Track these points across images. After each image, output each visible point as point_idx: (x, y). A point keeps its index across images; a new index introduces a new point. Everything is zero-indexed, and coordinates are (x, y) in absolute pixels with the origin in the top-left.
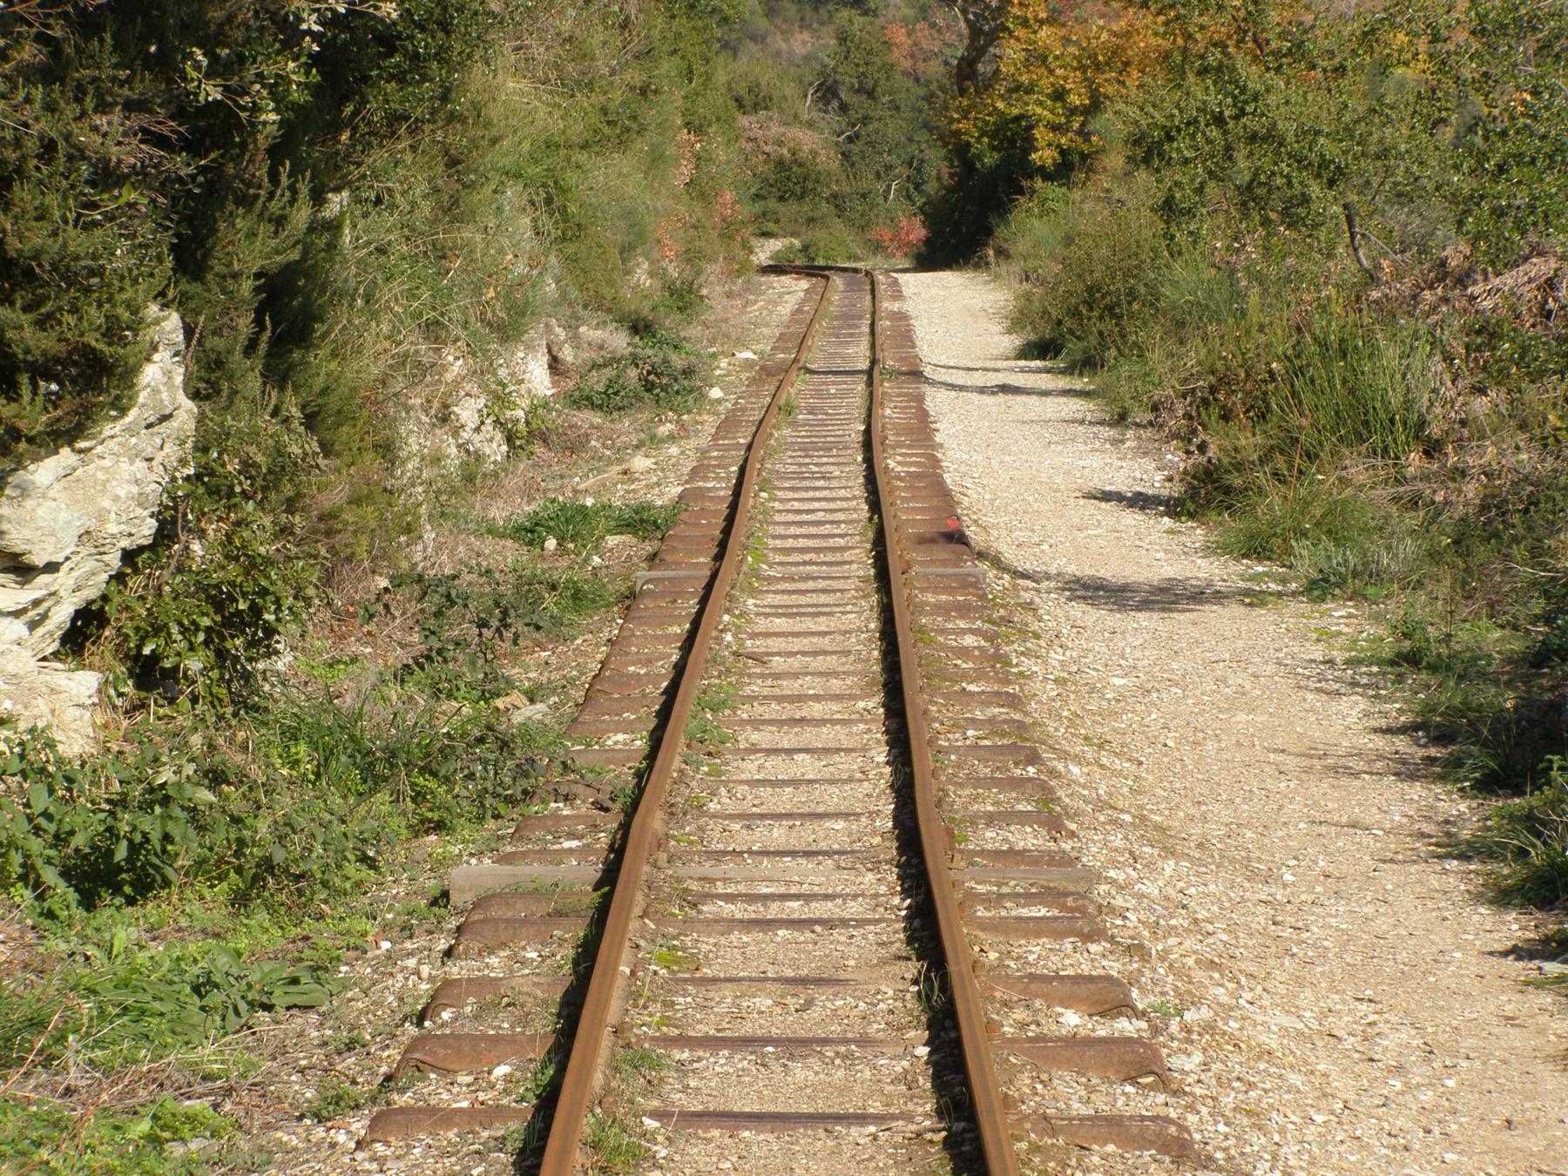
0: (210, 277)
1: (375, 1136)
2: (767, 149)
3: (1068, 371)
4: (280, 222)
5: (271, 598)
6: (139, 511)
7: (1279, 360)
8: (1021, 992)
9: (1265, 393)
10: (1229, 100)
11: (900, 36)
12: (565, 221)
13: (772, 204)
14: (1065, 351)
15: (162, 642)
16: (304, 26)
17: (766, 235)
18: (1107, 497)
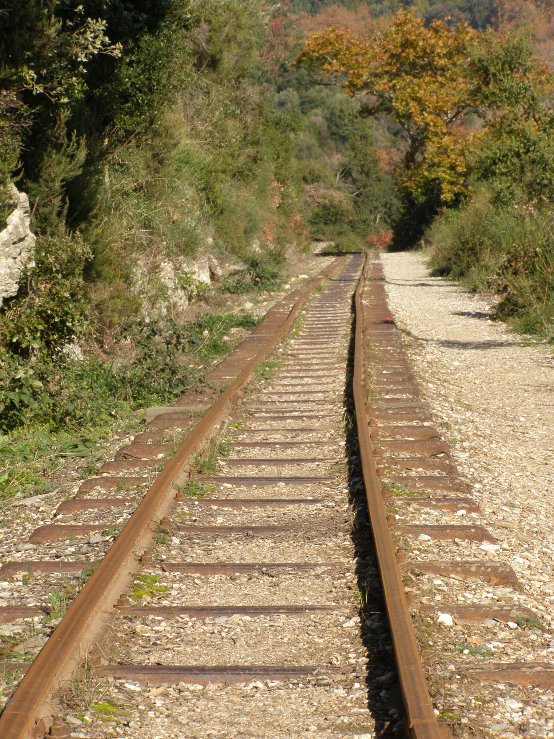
0: (41, 180)
1: (104, 470)
2: (318, 200)
3: (454, 280)
4: (72, 157)
5: (69, 316)
6: (10, 281)
7: (540, 247)
8: (390, 432)
9: (534, 262)
10: (522, 145)
11: (384, 155)
12: (216, 207)
13: (321, 226)
14: (452, 272)
15: (21, 336)
16: (79, 59)
17: (319, 240)
18: (463, 314)
